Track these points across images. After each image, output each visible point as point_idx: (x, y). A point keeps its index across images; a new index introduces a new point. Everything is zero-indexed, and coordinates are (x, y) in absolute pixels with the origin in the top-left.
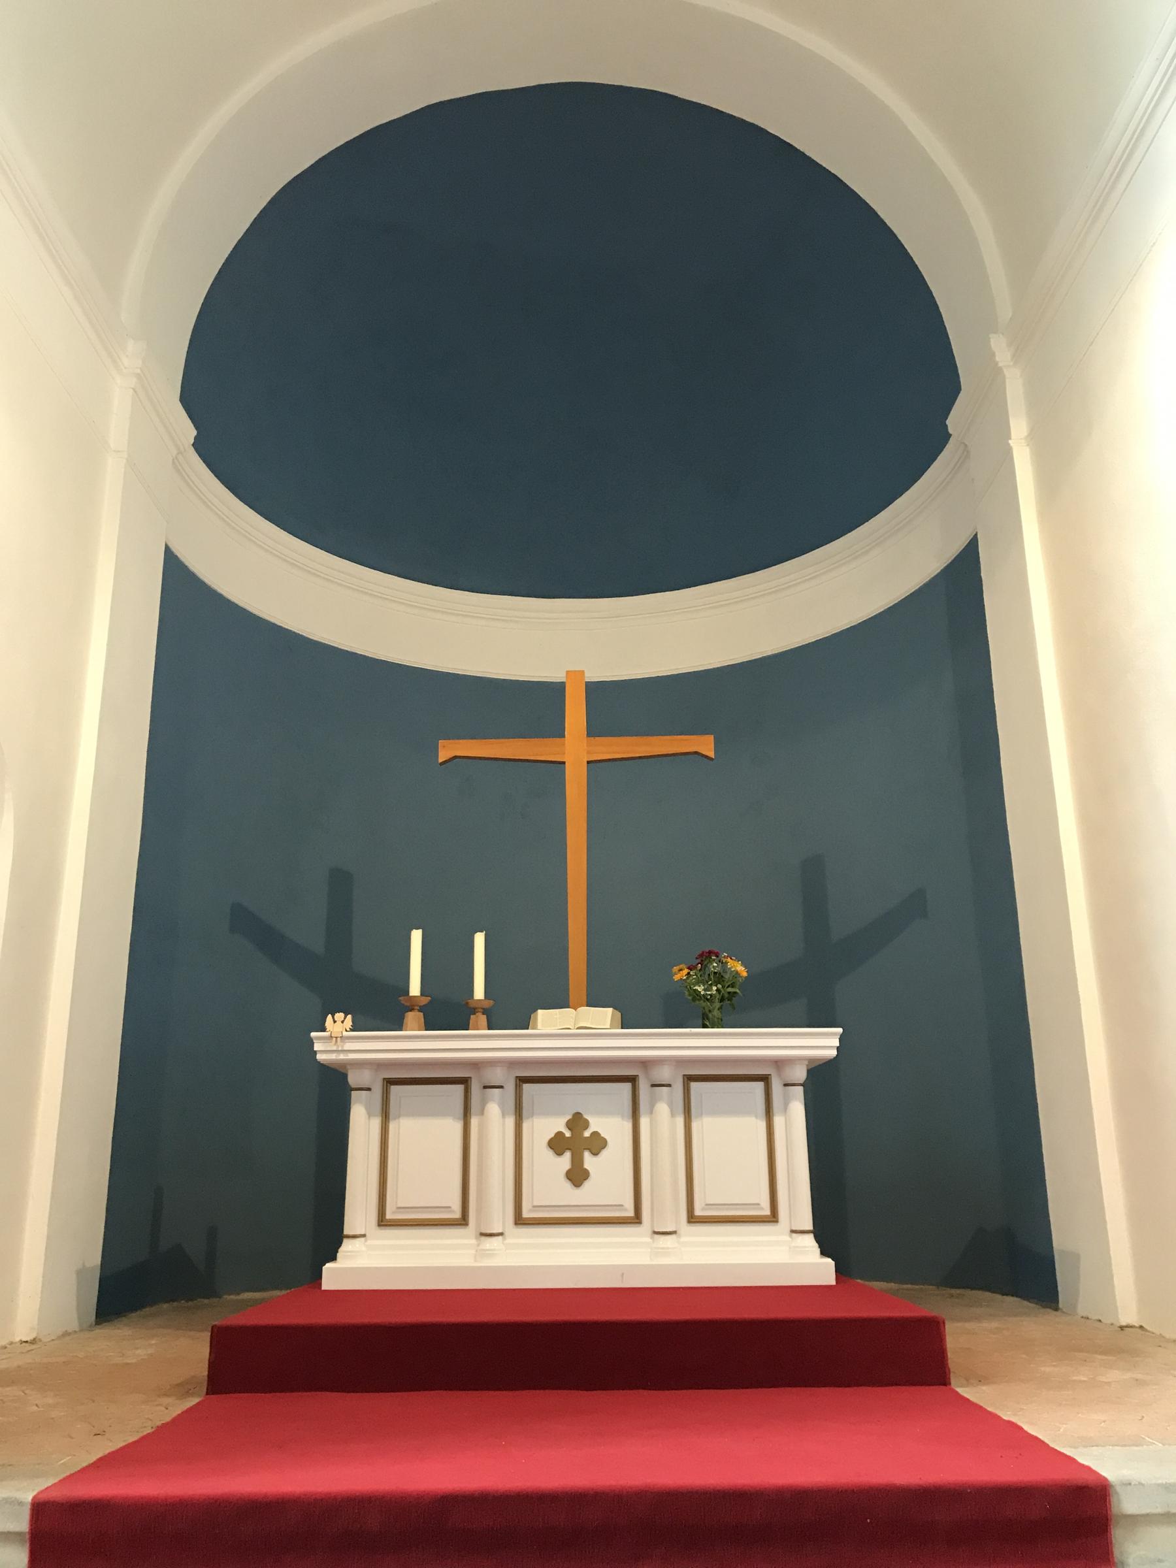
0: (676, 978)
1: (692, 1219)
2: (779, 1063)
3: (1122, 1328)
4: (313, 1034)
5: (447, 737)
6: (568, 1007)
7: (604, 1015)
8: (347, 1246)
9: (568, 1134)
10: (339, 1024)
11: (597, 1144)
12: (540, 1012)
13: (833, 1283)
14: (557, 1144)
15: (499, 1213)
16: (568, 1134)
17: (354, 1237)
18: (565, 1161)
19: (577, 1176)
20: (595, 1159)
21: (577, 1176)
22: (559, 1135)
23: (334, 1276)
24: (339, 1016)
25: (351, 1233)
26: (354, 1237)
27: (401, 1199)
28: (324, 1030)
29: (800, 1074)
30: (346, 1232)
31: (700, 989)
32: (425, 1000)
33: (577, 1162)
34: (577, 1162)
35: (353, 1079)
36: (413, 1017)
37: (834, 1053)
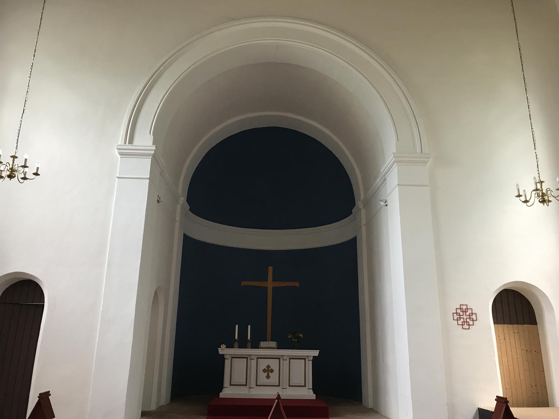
0: (289, 337)
1: (290, 386)
2: (308, 357)
3: (369, 408)
4: (218, 349)
5: (248, 338)
6: (266, 341)
7: (274, 344)
8: (224, 389)
9: (266, 369)
10: (223, 346)
11: (272, 371)
12: (261, 342)
13: (315, 399)
14: (264, 371)
15: (253, 384)
16: (266, 369)
17: (225, 387)
18: (266, 374)
19: (268, 377)
20: (272, 374)
21: (268, 377)
22: (265, 369)
23: (222, 395)
24: (223, 345)
25: (225, 387)
26: (225, 387)
27: (234, 381)
28: (220, 348)
29: (311, 358)
30: (148, 181)
31: (293, 340)
32: (238, 340)
33: (268, 374)
34: (268, 374)
35: (225, 357)
36: (236, 344)
37: (318, 355)
